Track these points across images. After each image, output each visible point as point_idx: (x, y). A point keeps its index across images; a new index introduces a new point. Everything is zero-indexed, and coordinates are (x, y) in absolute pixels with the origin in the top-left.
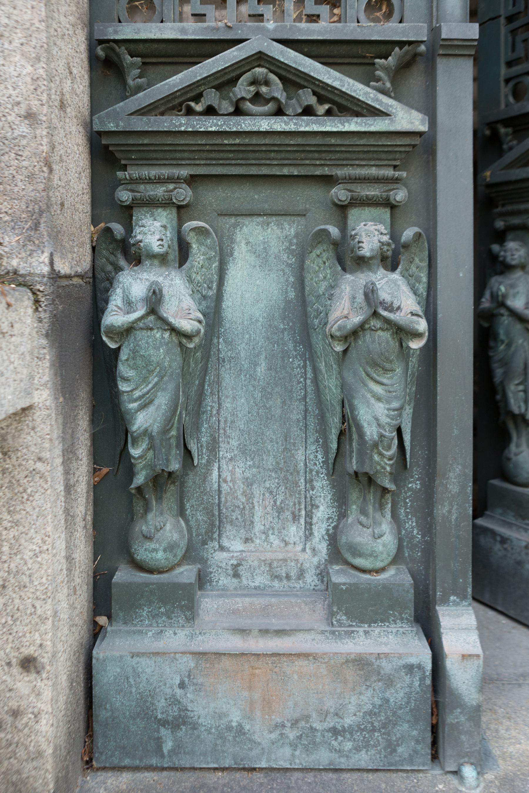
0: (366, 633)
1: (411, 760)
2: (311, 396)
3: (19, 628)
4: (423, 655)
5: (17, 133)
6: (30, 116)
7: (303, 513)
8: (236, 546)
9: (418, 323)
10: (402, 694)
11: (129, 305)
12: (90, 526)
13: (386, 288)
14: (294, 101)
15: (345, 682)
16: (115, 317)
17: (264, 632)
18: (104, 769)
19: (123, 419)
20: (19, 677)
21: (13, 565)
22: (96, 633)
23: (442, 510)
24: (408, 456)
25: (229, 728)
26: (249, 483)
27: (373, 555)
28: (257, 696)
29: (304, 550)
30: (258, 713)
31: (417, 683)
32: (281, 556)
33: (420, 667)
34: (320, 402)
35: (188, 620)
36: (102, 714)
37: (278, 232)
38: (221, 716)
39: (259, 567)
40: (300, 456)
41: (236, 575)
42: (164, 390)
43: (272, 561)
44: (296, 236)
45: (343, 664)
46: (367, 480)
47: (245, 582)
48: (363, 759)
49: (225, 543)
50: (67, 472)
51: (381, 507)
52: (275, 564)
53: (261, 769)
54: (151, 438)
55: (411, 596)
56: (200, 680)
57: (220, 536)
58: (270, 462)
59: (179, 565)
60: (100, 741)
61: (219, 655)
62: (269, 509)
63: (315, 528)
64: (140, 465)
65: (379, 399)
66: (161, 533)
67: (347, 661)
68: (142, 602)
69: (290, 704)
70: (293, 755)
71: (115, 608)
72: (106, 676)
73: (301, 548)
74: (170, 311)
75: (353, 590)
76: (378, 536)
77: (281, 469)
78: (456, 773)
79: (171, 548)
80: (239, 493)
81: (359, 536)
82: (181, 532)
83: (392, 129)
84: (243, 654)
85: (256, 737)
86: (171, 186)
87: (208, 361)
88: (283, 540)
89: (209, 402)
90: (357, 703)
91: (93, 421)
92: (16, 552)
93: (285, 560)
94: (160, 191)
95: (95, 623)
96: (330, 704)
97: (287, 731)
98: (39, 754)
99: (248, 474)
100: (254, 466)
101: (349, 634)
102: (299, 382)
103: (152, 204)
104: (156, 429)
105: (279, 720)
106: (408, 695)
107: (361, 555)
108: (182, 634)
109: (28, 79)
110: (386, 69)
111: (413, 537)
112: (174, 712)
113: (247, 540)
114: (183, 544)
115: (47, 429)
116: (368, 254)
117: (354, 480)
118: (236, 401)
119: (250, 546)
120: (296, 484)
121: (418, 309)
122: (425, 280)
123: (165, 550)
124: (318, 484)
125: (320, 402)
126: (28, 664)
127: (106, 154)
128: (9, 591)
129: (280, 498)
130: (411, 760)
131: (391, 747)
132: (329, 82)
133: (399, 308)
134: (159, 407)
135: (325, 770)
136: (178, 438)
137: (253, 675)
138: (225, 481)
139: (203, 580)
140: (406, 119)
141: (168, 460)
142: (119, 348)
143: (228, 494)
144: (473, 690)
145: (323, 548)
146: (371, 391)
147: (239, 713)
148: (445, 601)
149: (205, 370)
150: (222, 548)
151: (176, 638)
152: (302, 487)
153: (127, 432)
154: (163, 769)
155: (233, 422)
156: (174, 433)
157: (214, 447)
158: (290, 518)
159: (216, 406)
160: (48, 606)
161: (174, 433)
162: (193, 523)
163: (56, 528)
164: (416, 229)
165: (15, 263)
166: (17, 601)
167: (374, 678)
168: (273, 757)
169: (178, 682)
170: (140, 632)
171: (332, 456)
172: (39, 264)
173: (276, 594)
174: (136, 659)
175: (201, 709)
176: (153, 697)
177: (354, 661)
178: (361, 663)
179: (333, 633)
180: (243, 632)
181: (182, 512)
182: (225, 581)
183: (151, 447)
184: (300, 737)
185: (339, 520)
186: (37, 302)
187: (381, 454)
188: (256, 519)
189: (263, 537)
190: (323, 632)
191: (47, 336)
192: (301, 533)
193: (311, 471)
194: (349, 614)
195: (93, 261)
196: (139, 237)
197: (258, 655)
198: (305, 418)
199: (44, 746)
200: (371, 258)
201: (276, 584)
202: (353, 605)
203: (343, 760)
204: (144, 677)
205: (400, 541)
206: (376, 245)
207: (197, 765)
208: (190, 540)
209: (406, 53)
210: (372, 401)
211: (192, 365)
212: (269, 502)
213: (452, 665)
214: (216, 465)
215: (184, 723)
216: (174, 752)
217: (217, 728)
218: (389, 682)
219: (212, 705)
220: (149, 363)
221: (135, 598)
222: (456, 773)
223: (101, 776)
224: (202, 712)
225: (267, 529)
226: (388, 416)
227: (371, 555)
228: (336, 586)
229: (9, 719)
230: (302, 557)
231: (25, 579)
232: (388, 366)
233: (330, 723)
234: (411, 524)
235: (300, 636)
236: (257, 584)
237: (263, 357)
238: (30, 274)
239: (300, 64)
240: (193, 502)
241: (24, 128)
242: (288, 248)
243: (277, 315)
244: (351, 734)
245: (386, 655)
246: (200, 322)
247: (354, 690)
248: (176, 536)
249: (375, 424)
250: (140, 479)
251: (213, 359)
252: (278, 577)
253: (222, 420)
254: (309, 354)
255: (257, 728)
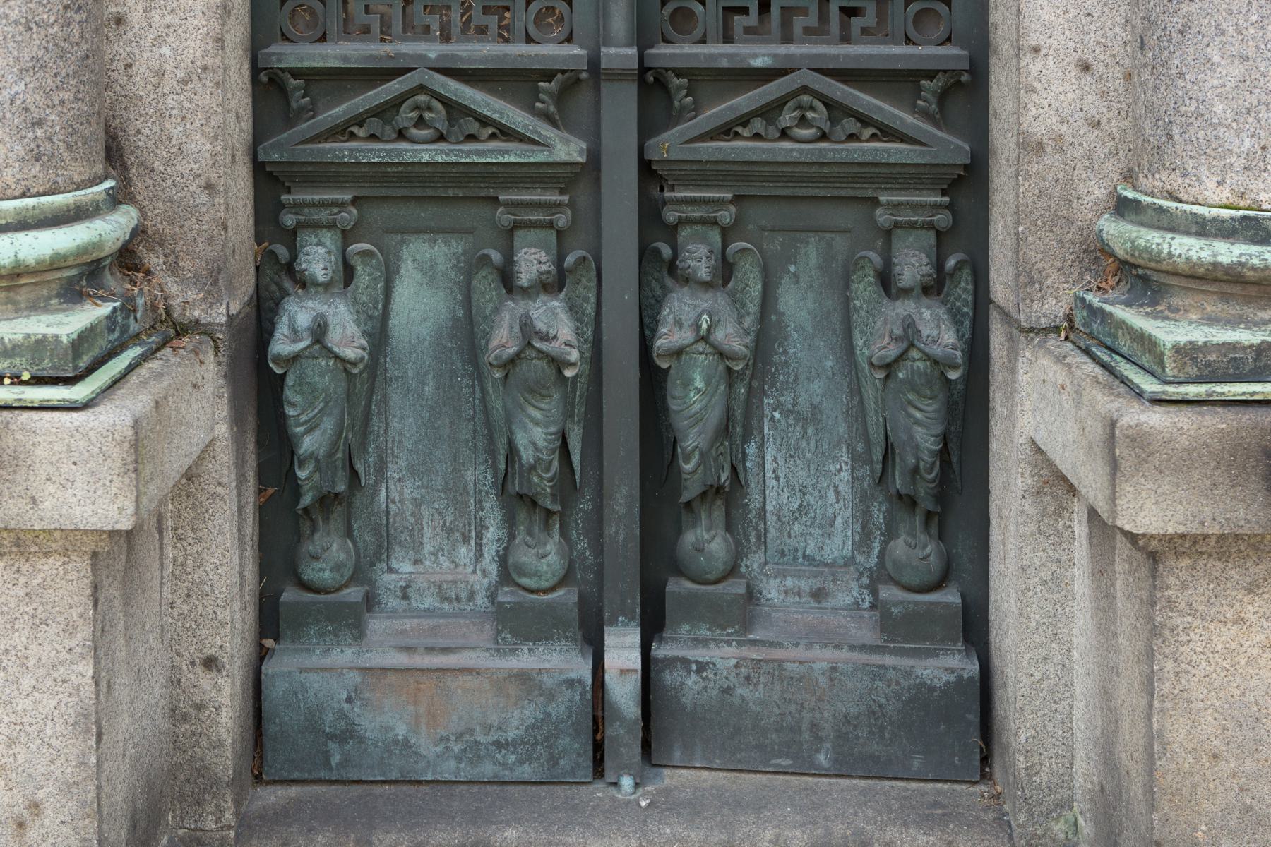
0: (530, 650)
1: (573, 772)
2: (480, 416)
3: (202, 632)
4: (582, 668)
5: (197, 201)
6: (209, 187)
7: (473, 534)
8: (406, 567)
9: (569, 354)
10: (563, 709)
11: (295, 335)
12: (256, 547)
13: (543, 317)
14: (456, 128)
15: (508, 696)
16: (281, 345)
17: (430, 650)
18: (275, 782)
19: (289, 440)
20: (202, 675)
21: (196, 577)
22: (262, 655)
23: (609, 530)
24: (577, 477)
25: (395, 742)
26: (418, 503)
27: (537, 574)
28: (422, 710)
29: (474, 572)
30: (424, 727)
31: (578, 698)
32: (450, 578)
33: (580, 681)
34: (488, 422)
35: (354, 638)
36: (270, 728)
37: (445, 249)
38: (388, 729)
39: (429, 588)
40: (469, 476)
41: (405, 597)
42: (329, 415)
43: (442, 583)
44: (464, 253)
45: (505, 679)
46: (532, 503)
47: (414, 604)
48: (527, 772)
49: (394, 565)
50: (239, 495)
51: (547, 527)
52: (445, 586)
53: (428, 782)
54: (317, 461)
55: (575, 614)
56: (367, 695)
57: (388, 557)
58: (439, 482)
59: (346, 586)
60: (269, 755)
61: (385, 670)
62: (438, 530)
63: (485, 550)
64: (306, 486)
65: (537, 424)
66: (328, 554)
67: (510, 676)
68: (310, 620)
69: (455, 718)
70: (458, 768)
71: (283, 625)
72: (275, 691)
73: (470, 567)
74: (334, 338)
75: (518, 608)
76: (544, 557)
77: (450, 490)
78: (615, 784)
79: (338, 568)
80: (408, 513)
81: (524, 556)
82: (348, 552)
83: (551, 160)
84: (408, 669)
85: (422, 751)
86: (335, 210)
87: (374, 381)
88: (453, 562)
89: (376, 421)
90: (518, 718)
91: (259, 443)
92: (199, 564)
93: (455, 582)
94: (325, 215)
95: (262, 646)
96: (493, 718)
97: (452, 744)
98: (220, 743)
99: (416, 495)
100: (423, 486)
101: (514, 652)
102: (468, 402)
103: (316, 226)
104: (322, 452)
105: (444, 734)
106: (569, 709)
107: (525, 575)
108: (349, 652)
109: (208, 155)
110: (546, 92)
111: (586, 559)
112: (341, 726)
113: (416, 562)
114: (350, 564)
115: (226, 459)
116: (526, 285)
117: (519, 503)
118: (402, 422)
119: (420, 568)
120: (466, 505)
121: (572, 338)
122: (593, 300)
123: (331, 570)
124: (487, 505)
125: (488, 422)
126: (210, 663)
127: (269, 181)
128: (193, 599)
129: (449, 519)
130: (573, 772)
131: (554, 760)
132: (489, 114)
133: (555, 337)
134: (325, 431)
135: (489, 782)
136: (343, 460)
137: (418, 689)
138: (393, 502)
139: (371, 602)
140: (567, 149)
141: (333, 482)
142: (285, 374)
143: (396, 515)
144: (631, 704)
145: (493, 569)
146: (529, 416)
147: (404, 726)
148: (614, 622)
149: (371, 391)
150: (391, 570)
151: (343, 656)
152: (472, 508)
153: (293, 453)
154: (331, 782)
155: (400, 442)
156: (339, 455)
157: (381, 468)
158: (460, 539)
159: (383, 426)
160: (227, 612)
161: (339, 455)
162: (360, 544)
163: (232, 544)
164: (581, 253)
165: (196, 313)
166: (200, 608)
167: (536, 693)
168: (439, 769)
169: (345, 696)
170: (308, 650)
171: (501, 477)
172: (219, 315)
173: (446, 615)
174: (304, 675)
175: (368, 723)
176: (320, 711)
177: (516, 676)
178: (523, 678)
179: (498, 650)
180: (409, 649)
181: (349, 533)
182: (393, 603)
183: (318, 469)
184: (464, 751)
185: (509, 541)
186: (216, 348)
187: (540, 476)
188: (426, 540)
189: (433, 558)
190: (488, 650)
191: (225, 377)
192: (472, 555)
193: (480, 491)
194: (515, 634)
195: (257, 280)
196: (304, 266)
197: (422, 670)
198: (474, 438)
199: (224, 737)
200: (529, 288)
201: (446, 606)
202: (518, 622)
203: (507, 773)
204: (312, 692)
205: (571, 563)
206: (534, 274)
207: (364, 778)
208: (358, 561)
209: (569, 78)
210: (531, 425)
211: (358, 386)
212: (438, 522)
213: (610, 678)
214: (384, 485)
215: (352, 737)
216: (341, 765)
217: (383, 742)
218: (551, 696)
219: (378, 719)
220: (314, 389)
221: (302, 618)
222: (615, 784)
223: (270, 789)
224: (369, 726)
225: (440, 551)
226: (545, 440)
227: (535, 575)
228: (501, 604)
229: (193, 712)
230: (472, 578)
231: (207, 589)
232: (544, 392)
233: (494, 737)
234: (583, 545)
235: (466, 654)
236: (426, 606)
237: (431, 376)
238: (210, 323)
239: (461, 97)
240: (360, 522)
241: (204, 198)
242: (455, 266)
243: (444, 333)
244: (515, 747)
245: (548, 670)
246: (364, 349)
247: (516, 704)
248: (342, 556)
249: (531, 447)
250: (306, 500)
251: (380, 379)
252: (449, 600)
253: (390, 440)
254: (477, 372)
255: (423, 741)
